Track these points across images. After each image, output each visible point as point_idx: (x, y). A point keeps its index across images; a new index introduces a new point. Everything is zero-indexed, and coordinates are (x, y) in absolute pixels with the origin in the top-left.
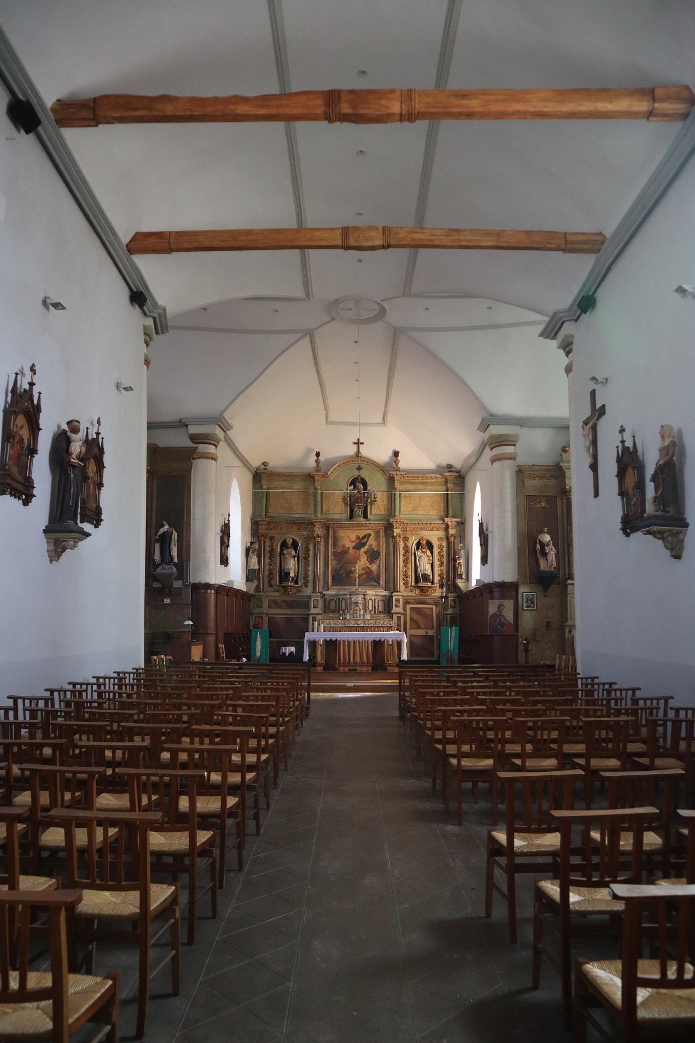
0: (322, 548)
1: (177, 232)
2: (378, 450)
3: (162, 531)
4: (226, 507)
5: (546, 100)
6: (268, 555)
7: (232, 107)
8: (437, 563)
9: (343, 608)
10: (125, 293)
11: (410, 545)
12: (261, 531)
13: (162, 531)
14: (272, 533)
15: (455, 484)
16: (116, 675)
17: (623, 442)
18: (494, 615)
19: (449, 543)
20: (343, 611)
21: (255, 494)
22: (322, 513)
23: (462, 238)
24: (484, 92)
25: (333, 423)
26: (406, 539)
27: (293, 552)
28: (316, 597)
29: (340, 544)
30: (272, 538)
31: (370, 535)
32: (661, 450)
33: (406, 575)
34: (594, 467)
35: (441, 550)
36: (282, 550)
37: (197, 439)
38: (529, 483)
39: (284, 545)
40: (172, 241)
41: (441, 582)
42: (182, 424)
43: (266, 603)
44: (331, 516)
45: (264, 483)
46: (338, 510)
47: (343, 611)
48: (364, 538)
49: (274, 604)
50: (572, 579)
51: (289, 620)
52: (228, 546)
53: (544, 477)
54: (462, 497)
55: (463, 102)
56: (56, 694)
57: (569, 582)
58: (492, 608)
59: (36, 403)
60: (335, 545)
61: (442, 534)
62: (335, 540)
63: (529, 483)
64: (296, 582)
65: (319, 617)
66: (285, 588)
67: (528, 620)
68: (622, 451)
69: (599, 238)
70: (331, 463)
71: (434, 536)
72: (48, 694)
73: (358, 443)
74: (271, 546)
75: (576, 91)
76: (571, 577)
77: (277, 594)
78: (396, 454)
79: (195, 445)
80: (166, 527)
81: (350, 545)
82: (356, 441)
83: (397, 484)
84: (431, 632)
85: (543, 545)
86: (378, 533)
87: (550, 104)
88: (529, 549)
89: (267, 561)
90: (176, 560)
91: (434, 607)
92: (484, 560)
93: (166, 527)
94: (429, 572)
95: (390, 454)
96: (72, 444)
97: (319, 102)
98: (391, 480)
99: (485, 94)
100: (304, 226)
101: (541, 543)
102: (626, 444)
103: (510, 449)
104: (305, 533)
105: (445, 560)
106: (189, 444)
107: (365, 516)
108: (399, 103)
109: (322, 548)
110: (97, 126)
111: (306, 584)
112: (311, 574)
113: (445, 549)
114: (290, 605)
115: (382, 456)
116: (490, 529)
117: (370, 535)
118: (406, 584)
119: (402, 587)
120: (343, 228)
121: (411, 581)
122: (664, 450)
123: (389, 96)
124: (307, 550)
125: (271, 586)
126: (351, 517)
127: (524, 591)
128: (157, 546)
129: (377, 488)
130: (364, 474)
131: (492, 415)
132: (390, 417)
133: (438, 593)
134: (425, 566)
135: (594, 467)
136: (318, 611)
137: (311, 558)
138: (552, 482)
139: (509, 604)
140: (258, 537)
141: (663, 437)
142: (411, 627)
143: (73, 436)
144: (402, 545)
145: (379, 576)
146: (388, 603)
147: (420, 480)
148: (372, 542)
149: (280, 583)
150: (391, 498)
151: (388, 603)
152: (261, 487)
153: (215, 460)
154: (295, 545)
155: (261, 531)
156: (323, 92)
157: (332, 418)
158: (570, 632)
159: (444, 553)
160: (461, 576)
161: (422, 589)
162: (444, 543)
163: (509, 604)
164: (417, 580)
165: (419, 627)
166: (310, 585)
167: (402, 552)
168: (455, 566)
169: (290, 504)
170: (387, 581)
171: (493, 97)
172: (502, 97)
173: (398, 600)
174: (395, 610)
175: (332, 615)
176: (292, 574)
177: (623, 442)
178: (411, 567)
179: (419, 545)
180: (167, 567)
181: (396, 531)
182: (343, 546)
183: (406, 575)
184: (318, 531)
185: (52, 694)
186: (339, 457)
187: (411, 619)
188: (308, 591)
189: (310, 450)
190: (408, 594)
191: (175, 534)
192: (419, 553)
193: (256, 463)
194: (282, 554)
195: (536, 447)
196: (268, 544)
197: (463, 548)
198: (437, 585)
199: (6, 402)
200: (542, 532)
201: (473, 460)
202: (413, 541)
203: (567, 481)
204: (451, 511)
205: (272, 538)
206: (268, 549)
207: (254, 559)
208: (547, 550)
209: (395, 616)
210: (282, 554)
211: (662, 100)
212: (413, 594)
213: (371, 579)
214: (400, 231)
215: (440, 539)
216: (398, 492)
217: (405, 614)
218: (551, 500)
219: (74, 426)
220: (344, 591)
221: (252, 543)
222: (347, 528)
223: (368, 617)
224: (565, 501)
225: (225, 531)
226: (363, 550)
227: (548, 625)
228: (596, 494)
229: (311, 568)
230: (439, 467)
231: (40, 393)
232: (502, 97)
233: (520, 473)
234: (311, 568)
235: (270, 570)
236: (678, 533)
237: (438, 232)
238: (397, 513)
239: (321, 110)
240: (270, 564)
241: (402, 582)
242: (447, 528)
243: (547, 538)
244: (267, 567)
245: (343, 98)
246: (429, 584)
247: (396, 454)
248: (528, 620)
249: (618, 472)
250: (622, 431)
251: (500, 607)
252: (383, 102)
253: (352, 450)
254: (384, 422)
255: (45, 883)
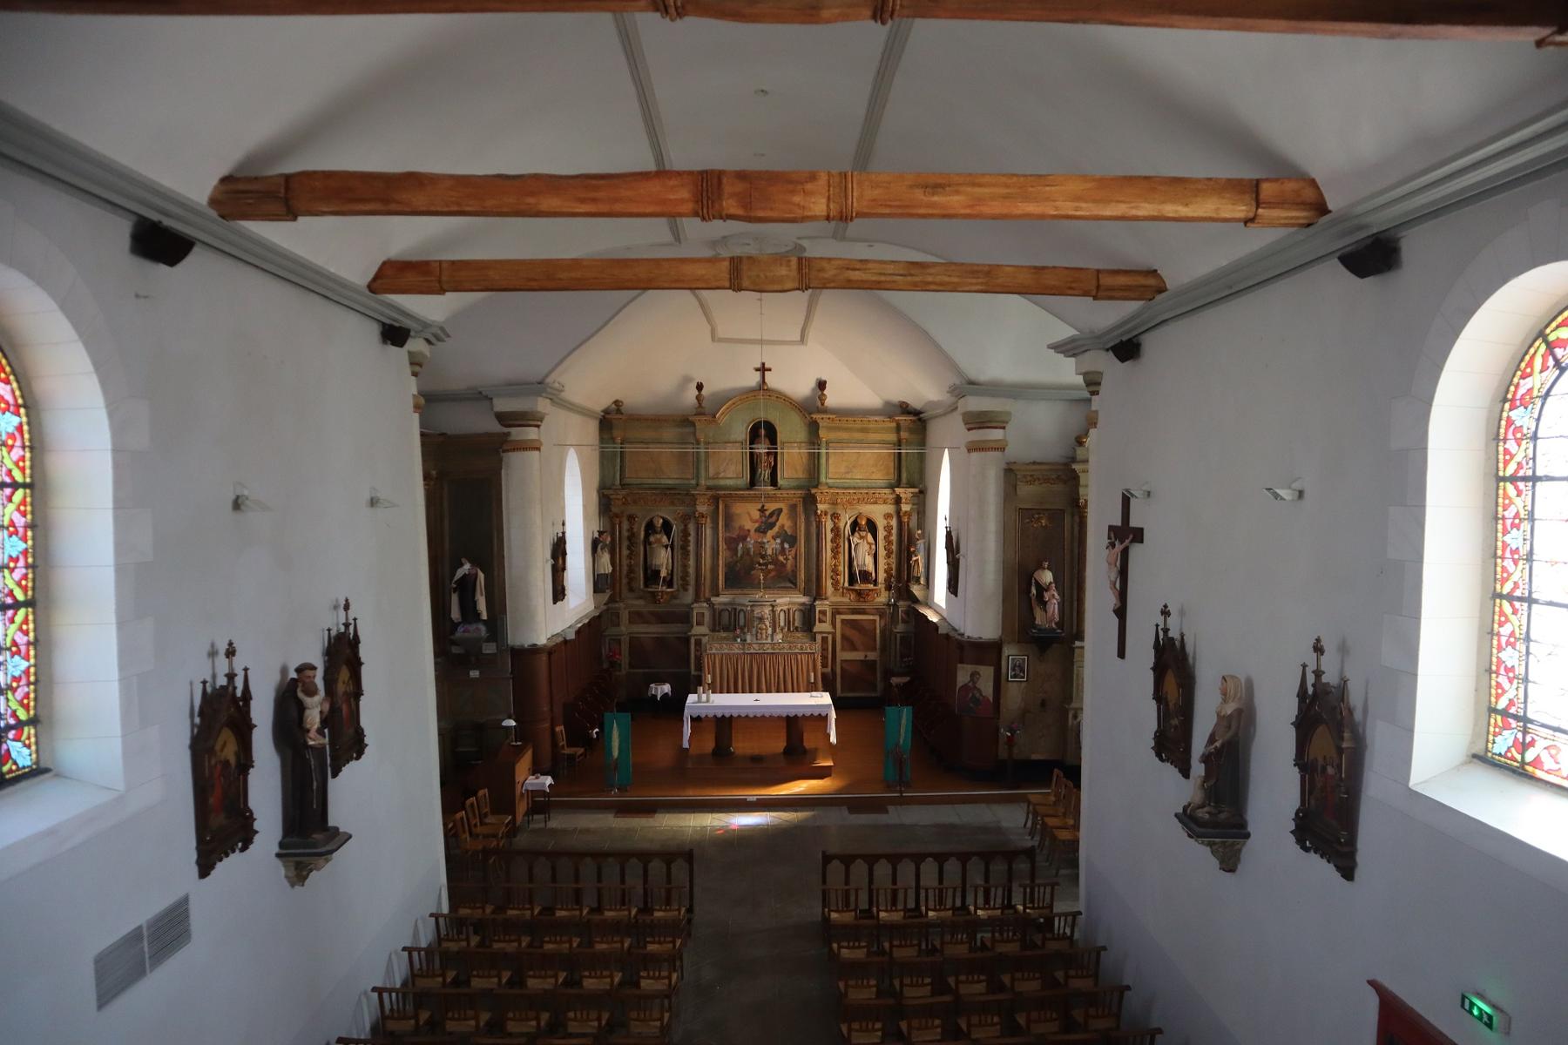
0: (709, 531)
1: (453, 263)
2: (794, 380)
3: (460, 573)
4: (561, 503)
5: (1078, 198)
6: (625, 543)
7: (531, 200)
8: (882, 553)
9: (742, 622)
11: (841, 525)
12: (615, 510)
13: (460, 573)
14: (632, 509)
15: (911, 431)
18: (965, 687)
19: (900, 523)
20: (742, 629)
21: (603, 456)
22: (708, 478)
23: (930, 279)
24: (973, 180)
25: (721, 340)
26: (835, 516)
27: (665, 539)
28: (701, 608)
29: (736, 525)
30: (631, 518)
31: (780, 511)
32: (1220, 717)
33: (835, 571)
34: (1121, 612)
35: (890, 533)
36: (647, 535)
37: (506, 419)
38: (1025, 490)
39: (650, 527)
40: (444, 278)
41: (888, 580)
42: (479, 397)
43: (625, 616)
44: (722, 482)
45: (618, 434)
46: (730, 467)
47: (742, 629)
48: (771, 515)
49: (637, 617)
50: (1081, 638)
51: (660, 641)
52: (564, 569)
53: (1047, 480)
54: (922, 458)
55: (936, 198)
57: (1077, 643)
58: (963, 676)
59: (239, 693)
60: (727, 526)
61: (890, 509)
62: (729, 519)
63: (1025, 490)
64: (670, 584)
65: (705, 640)
66: (654, 594)
67: (1015, 695)
69: (1151, 281)
70: (724, 399)
71: (879, 512)
73: (763, 369)
74: (630, 530)
75: (1130, 180)
76: (1080, 636)
77: (641, 602)
78: (822, 385)
79: (506, 430)
80: (467, 566)
81: (749, 526)
82: (759, 365)
83: (822, 433)
84: (872, 656)
85: (1041, 589)
86: (793, 507)
87: (1084, 205)
88: (1020, 590)
89: (625, 552)
90: (484, 616)
91: (877, 618)
92: (953, 586)
93: (467, 566)
94: (871, 568)
95: (812, 384)
96: (308, 712)
97: (684, 194)
98: (813, 427)
99: (974, 185)
100: (668, 168)
101: (1038, 585)
103: (996, 434)
104: (681, 509)
105: (894, 547)
106: (495, 427)
107: (774, 482)
108: (824, 201)
109: (708, 532)
110: (295, 219)
111: (685, 587)
112: (691, 570)
113: (894, 531)
114: (662, 618)
115: (800, 387)
116: (962, 550)
117: (780, 511)
118: (835, 584)
119: (830, 589)
120: (732, 259)
121: (844, 580)
122: (1224, 721)
123: (809, 186)
124: (686, 534)
125: (631, 590)
126: (753, 483)
127: (1010, 652)
128: (455, 598)
129: (791, 430)
130: (774, 417)
131: (971, 383)
132: (812, 334)
133: (882, 598)
134: (865, 560)
135: (1121, 612)
136: (703, 630)
137: (691, 548)
138: (1058, 487)
139: (987, 672)
140: (611, 519)
141: (1224, 693)
142: (843, 649)
143: (308, 701)
144: (829, 525)
145: (795, 573)
146: (808, 617)
147: (858, 425)
148: (784, 521)
149: (646, 585)
150: (814, 460)
151: (808, 617)
152: (613, 440)
153: (538, 449)
154: (667, 527)
155: (615, 510)
156: (691, 173)
157: (721, 333)
158: (1075, 717)
159: (894, 538)
160: (917, 580)
161: (859, 593)
162: (894, 522)
163: (987, 672)
164: (852, 580)
165: (854, 648)
166: (691, 589)
167: (829, 536)
168: (909, 566)
169: (661, 462)
170: (808, 581)
171: (987, 190)
172: (1005, 191)
173: (823, 613)
174: (818, 627)
175: (724, 635)
176: (663, 573)
178: (843, 559)
179: (855, 526)
180: (472, 627)
181: (821, 507)
182: (741, 528)
183: (835, 571)
184: (702, 508)
186: (734, 390)
187: (844, 637)
188: (688, 597)
189: (687, 380)
190: (839, 599)
191: (481, 576)
192: (855, 540)
193: (602, 402)
194: (647, 542)
195: (1036, 431)
196: (625, 526)
197: (922, 536)
198: (881, 586)
199: (193, 725)
200: (1040, 567)
201: (939, 411)
202: (846, 521)
203: (1082, 491)
204: (904, 476)
205: (631, 518)
206: (625, 534)
207: (605, 558)
208: (1047, 596)
209: (819, 637)
210: (647, 542)
211: (1271, 205)
212: (846, 600)
213: (784, 579)
214: (825, 264)
215: (887, 516)
216: (823, 451)
217: (834, 635)
218: (1056, 516)
220: (744, 599)
221: (601, 533)
222: (743, 499)
223: (779, 637)
224: (1077, 519)
225: (559, 550)
226: (770, 533)
227: (1043, 704)
228: (1121, 653)
229: (692, 562)
230: (888, 404)
231: (246, 670)
232: (1005, 191)
233: (1011, 474)
234: (692, 562)
235: (630, 566)
236: (1233, 844)
237: (890, 269)
238: (823, 479)
239: (689, 207)
240: (629, 557)
241: (829, 582)
242: (898, 501)
243: (1047, 577)
244: (625, 562)
245: (728, 188)
246: (871, 586)
247: (822, 385)
248: (1015, 695)
251: (974, 675)
252: (797, 199)
253: (753, 379)
254: (803, 340)
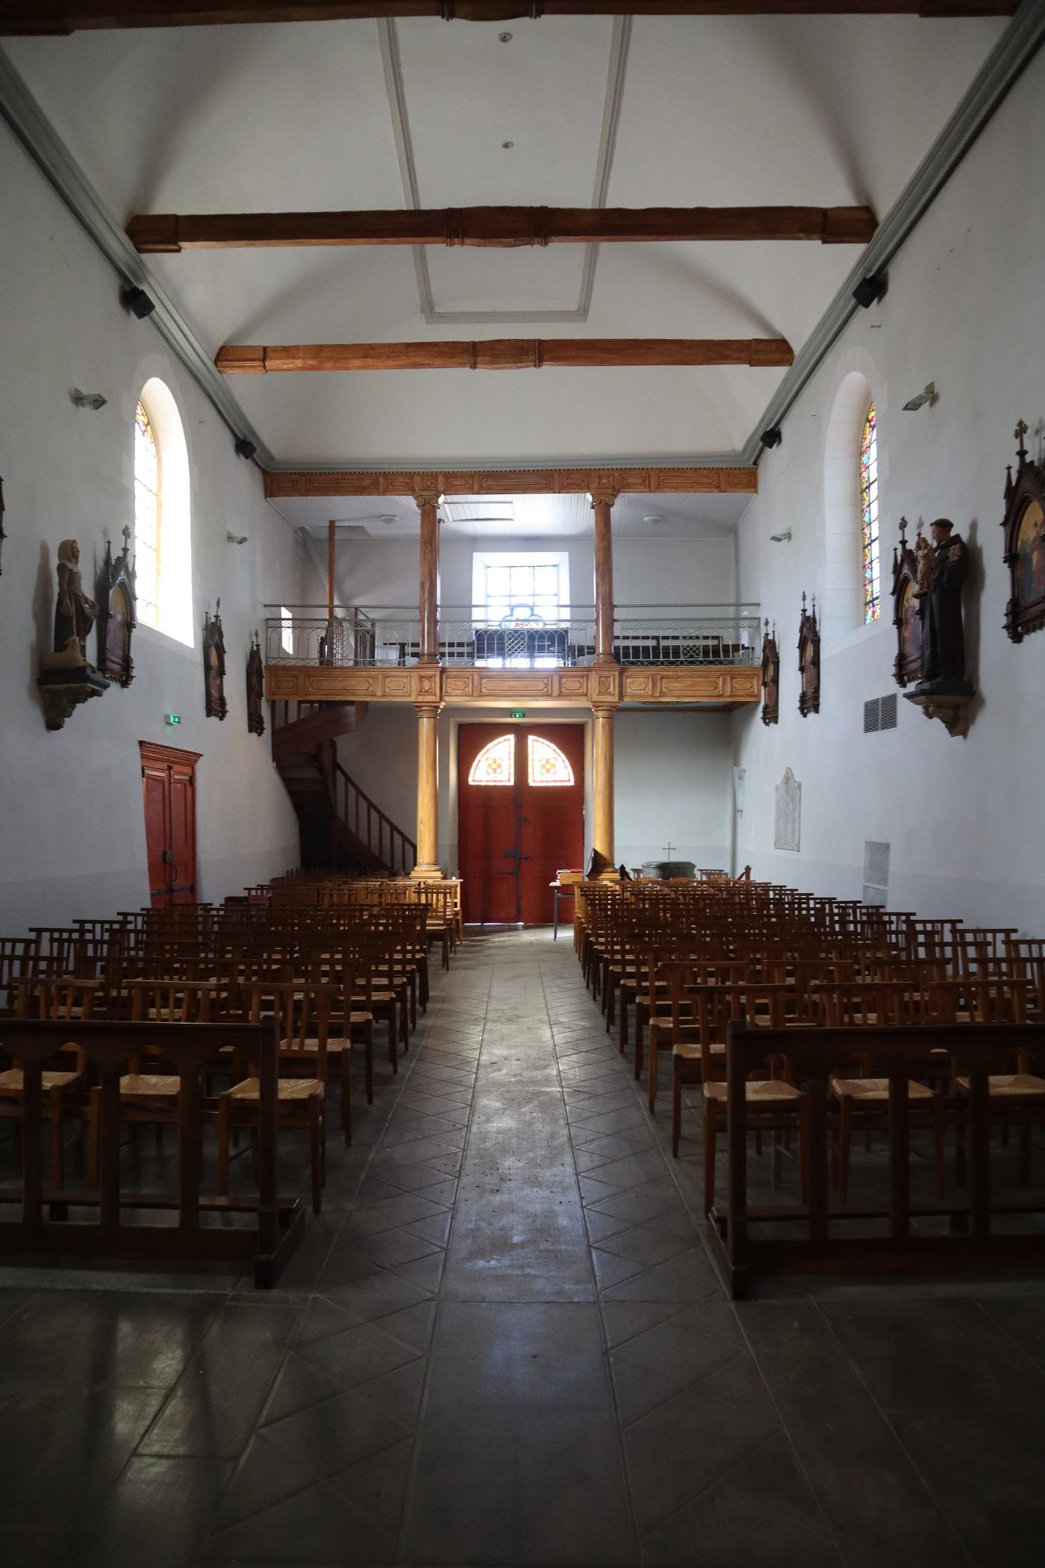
10: (229, 443)
16: (77, 926)
17: (903, 542)
56: (46, 936)
68: (1020, 473)
72: (33, 935)
102: (1028, 458)
177: (903, 542)
185: (39, 936)
219: (69, 551)
249: (1007, 517)
250: (903, 525)
255: (240, 1091)
